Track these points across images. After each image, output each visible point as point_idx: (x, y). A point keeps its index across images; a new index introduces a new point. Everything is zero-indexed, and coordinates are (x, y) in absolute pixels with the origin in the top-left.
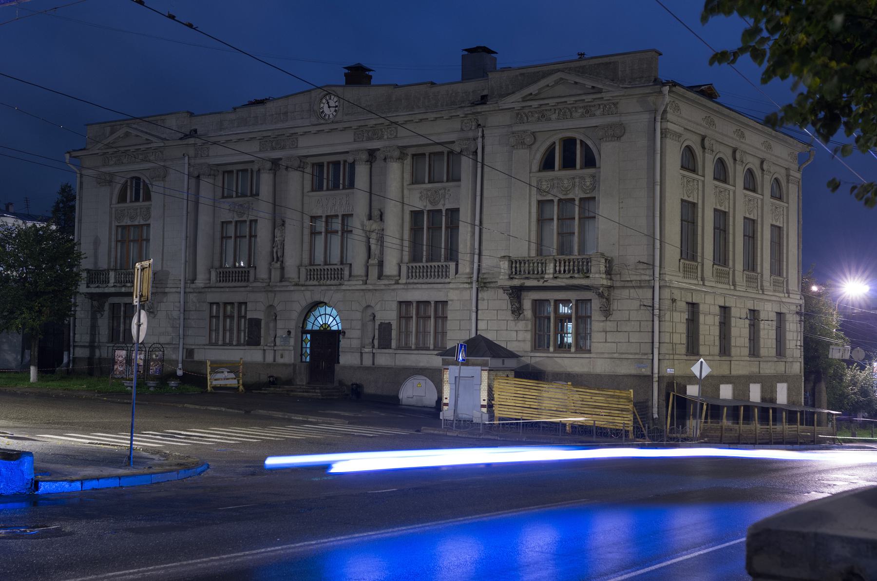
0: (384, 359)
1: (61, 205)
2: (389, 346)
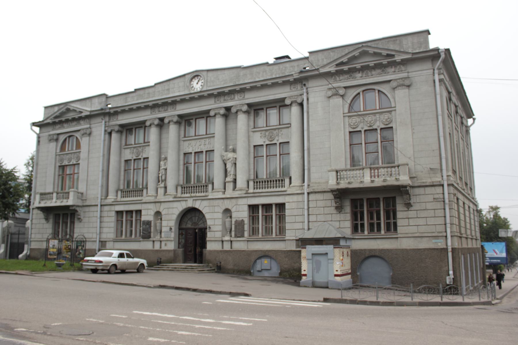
0: (240, 245)
2: (243, 236)
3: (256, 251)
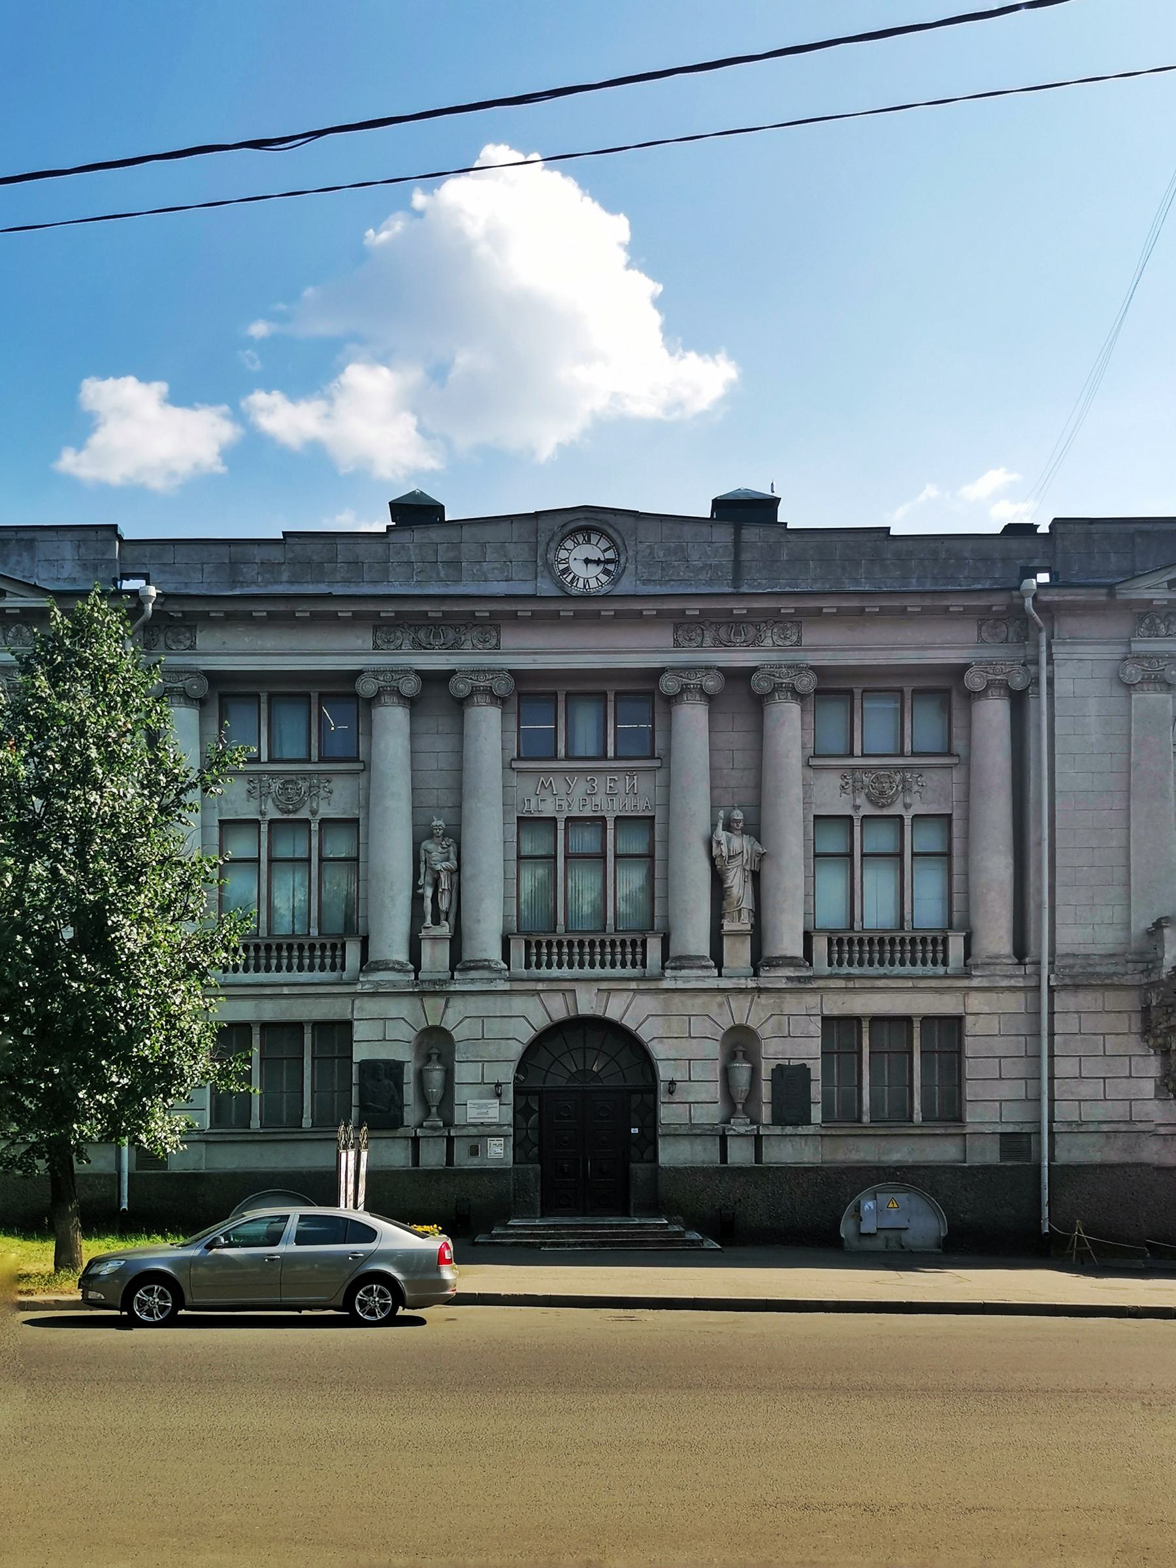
1: (783, 636)
3: (859, 1168)
